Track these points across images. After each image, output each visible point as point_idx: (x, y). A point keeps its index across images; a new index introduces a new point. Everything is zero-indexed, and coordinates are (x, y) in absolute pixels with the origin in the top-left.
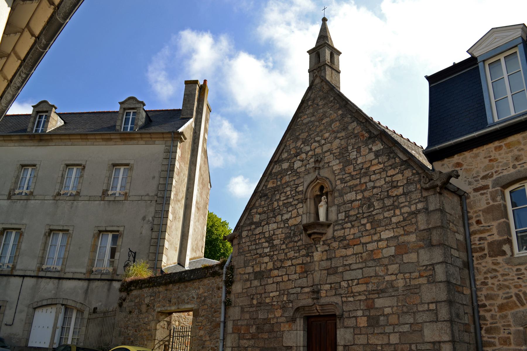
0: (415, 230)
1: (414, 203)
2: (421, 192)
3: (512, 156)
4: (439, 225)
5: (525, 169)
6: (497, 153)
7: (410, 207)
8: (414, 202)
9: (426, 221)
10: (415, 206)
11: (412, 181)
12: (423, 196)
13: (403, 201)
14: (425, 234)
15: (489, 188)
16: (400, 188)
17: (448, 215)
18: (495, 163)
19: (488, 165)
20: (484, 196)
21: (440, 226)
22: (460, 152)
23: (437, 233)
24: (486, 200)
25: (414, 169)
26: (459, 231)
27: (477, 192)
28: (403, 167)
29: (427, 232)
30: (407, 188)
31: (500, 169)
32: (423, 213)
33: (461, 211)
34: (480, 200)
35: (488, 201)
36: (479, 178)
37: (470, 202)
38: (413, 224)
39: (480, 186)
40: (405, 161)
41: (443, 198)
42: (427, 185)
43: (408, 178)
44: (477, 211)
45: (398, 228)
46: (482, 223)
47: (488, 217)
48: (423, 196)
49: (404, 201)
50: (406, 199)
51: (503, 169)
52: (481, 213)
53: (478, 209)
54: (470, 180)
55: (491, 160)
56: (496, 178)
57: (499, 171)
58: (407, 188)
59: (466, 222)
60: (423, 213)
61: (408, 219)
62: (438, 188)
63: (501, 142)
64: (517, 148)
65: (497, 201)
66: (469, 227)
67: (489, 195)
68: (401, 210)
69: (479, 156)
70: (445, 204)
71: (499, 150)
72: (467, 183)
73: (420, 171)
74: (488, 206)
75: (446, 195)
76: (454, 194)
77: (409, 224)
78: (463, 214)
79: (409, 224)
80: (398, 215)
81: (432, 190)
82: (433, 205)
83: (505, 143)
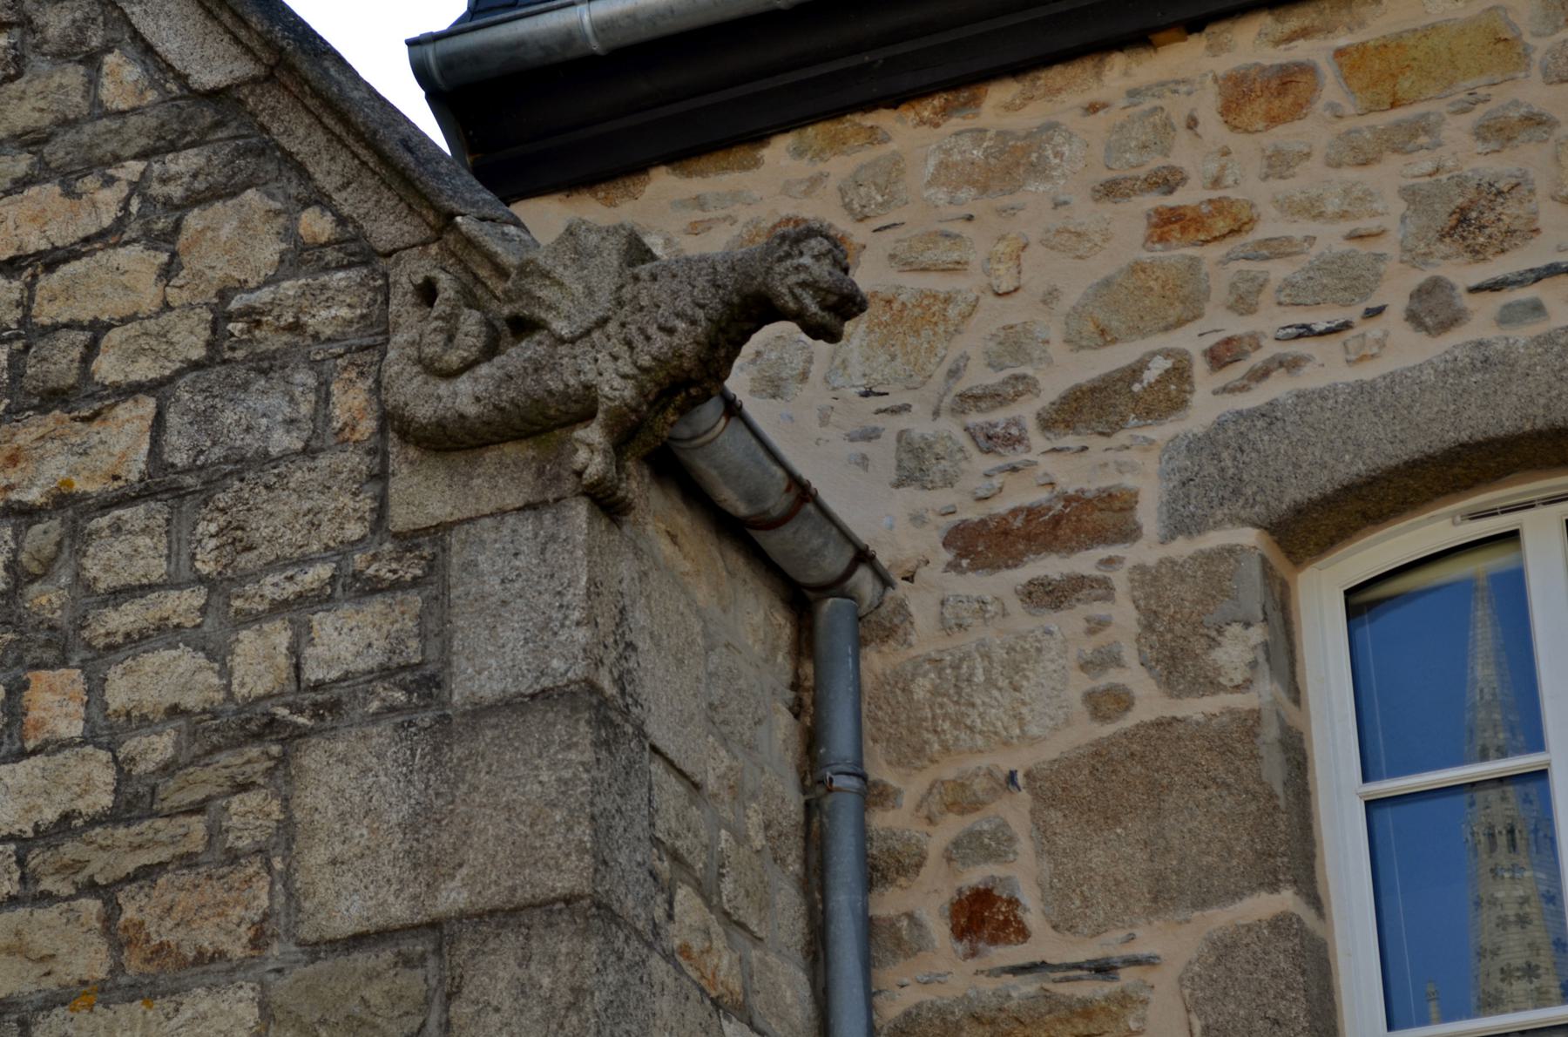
0: (259, 940)
1: (279, 608)
2: (380, 476)
3: (1410, 195)
4: (563, 883)
5: (1548, 340)
6: (1248, 148)
7: (219, 655)
8: (273, 587)
9: (410, 827)
10: (280, 635)
11: (270, 340)
12: (401, 517)
13: (131, 574)
14: (374, 993)
15: (1129, 533)
16: (123, 411)
17: (670, 791)
18: (1215, 252)
19: (1137, 268)
20: (1069, 622)
21: (569, 900)
22: (836, 113)
23: (523, 989)
24: (1085, 666)
25: (321, 200)
26: (757, 1002)
27: (994, 567)
28: (185, 162)
29: (407, 962)
30: (205, 418)
31: (1269, 320)
32: (382, 734)
33: (791, 777)
34: (1017, 664)
35: (1113, 677)
36: (1026, 411)
37: (902, 682)
38: (233, 857)
39: (1032, 496)
40: (215, 95)
41: (626, 568)
42: (464, 385)
43: (224, 295)
44: (980, 785)
45: (48, 898)
46: (1023, 933)
47: (1097, 858)
48: (401, 517)
49: (158, 569)
50: (177, 544)
51: (1306, 332)
52: (1016, 812)
53: (984, 761)
54: (920, 425)
55: (1168, 224)
56: (1221, 424)
57: (1255, 341)
58: (205, 418)
59: (843, 900)
60: (382, 734)
61: (175, 794)
62: (593, 433)
63: (1304, 33)
64: (1474, 101)
65: (1214, 686)
66: (868, 964)
67: (1123, 614)
68: (96, 686)
69: (1038, 170)
70: (644, 644)
71: (1273, 120)
72: (884, 453)
73: (387, 229)
74: (1107, 730)
75: (665, 547)
76: (737, 561)
77: (188, 861)
78: (809, 808)
79: (188, 861)
80: (63, 745)
81: (511, 450)
82: (510, 634)
83: (1342, 41)
